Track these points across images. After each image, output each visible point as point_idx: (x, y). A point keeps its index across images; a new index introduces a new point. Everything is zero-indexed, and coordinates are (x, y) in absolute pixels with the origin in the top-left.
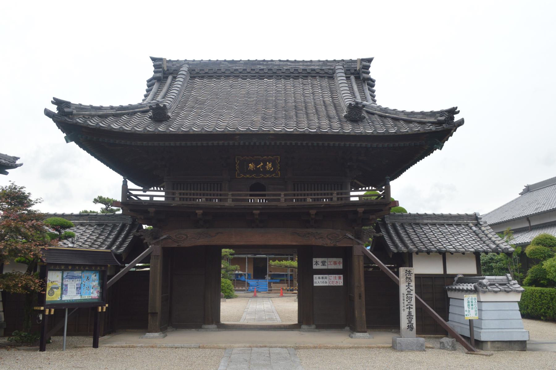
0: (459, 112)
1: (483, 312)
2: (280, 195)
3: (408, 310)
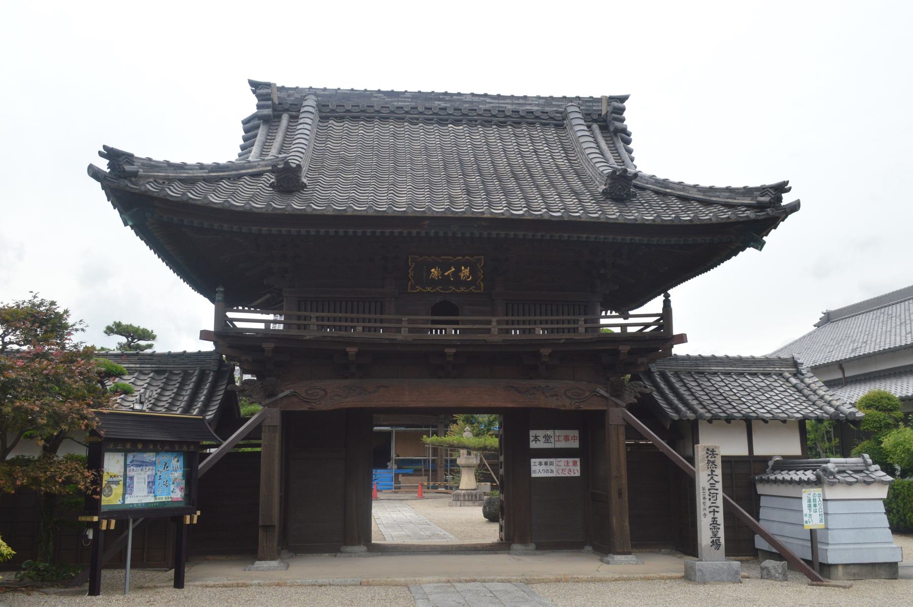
0: (790, 188)
1: (829, 517)
2: (489, 323)
3: (711, 515)
